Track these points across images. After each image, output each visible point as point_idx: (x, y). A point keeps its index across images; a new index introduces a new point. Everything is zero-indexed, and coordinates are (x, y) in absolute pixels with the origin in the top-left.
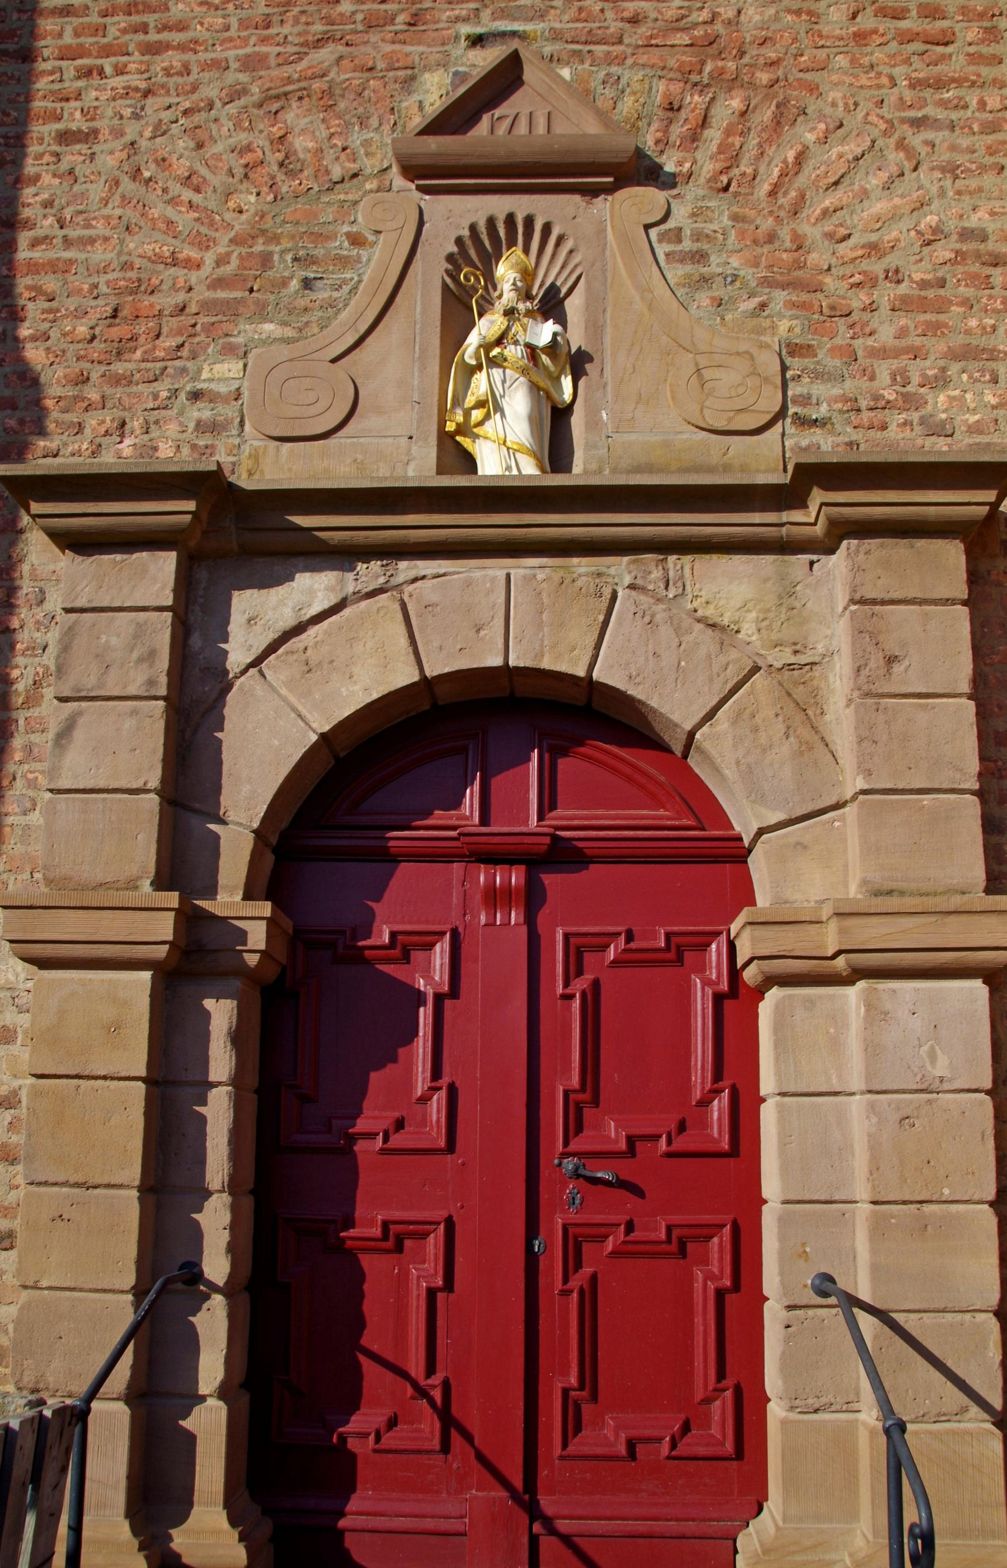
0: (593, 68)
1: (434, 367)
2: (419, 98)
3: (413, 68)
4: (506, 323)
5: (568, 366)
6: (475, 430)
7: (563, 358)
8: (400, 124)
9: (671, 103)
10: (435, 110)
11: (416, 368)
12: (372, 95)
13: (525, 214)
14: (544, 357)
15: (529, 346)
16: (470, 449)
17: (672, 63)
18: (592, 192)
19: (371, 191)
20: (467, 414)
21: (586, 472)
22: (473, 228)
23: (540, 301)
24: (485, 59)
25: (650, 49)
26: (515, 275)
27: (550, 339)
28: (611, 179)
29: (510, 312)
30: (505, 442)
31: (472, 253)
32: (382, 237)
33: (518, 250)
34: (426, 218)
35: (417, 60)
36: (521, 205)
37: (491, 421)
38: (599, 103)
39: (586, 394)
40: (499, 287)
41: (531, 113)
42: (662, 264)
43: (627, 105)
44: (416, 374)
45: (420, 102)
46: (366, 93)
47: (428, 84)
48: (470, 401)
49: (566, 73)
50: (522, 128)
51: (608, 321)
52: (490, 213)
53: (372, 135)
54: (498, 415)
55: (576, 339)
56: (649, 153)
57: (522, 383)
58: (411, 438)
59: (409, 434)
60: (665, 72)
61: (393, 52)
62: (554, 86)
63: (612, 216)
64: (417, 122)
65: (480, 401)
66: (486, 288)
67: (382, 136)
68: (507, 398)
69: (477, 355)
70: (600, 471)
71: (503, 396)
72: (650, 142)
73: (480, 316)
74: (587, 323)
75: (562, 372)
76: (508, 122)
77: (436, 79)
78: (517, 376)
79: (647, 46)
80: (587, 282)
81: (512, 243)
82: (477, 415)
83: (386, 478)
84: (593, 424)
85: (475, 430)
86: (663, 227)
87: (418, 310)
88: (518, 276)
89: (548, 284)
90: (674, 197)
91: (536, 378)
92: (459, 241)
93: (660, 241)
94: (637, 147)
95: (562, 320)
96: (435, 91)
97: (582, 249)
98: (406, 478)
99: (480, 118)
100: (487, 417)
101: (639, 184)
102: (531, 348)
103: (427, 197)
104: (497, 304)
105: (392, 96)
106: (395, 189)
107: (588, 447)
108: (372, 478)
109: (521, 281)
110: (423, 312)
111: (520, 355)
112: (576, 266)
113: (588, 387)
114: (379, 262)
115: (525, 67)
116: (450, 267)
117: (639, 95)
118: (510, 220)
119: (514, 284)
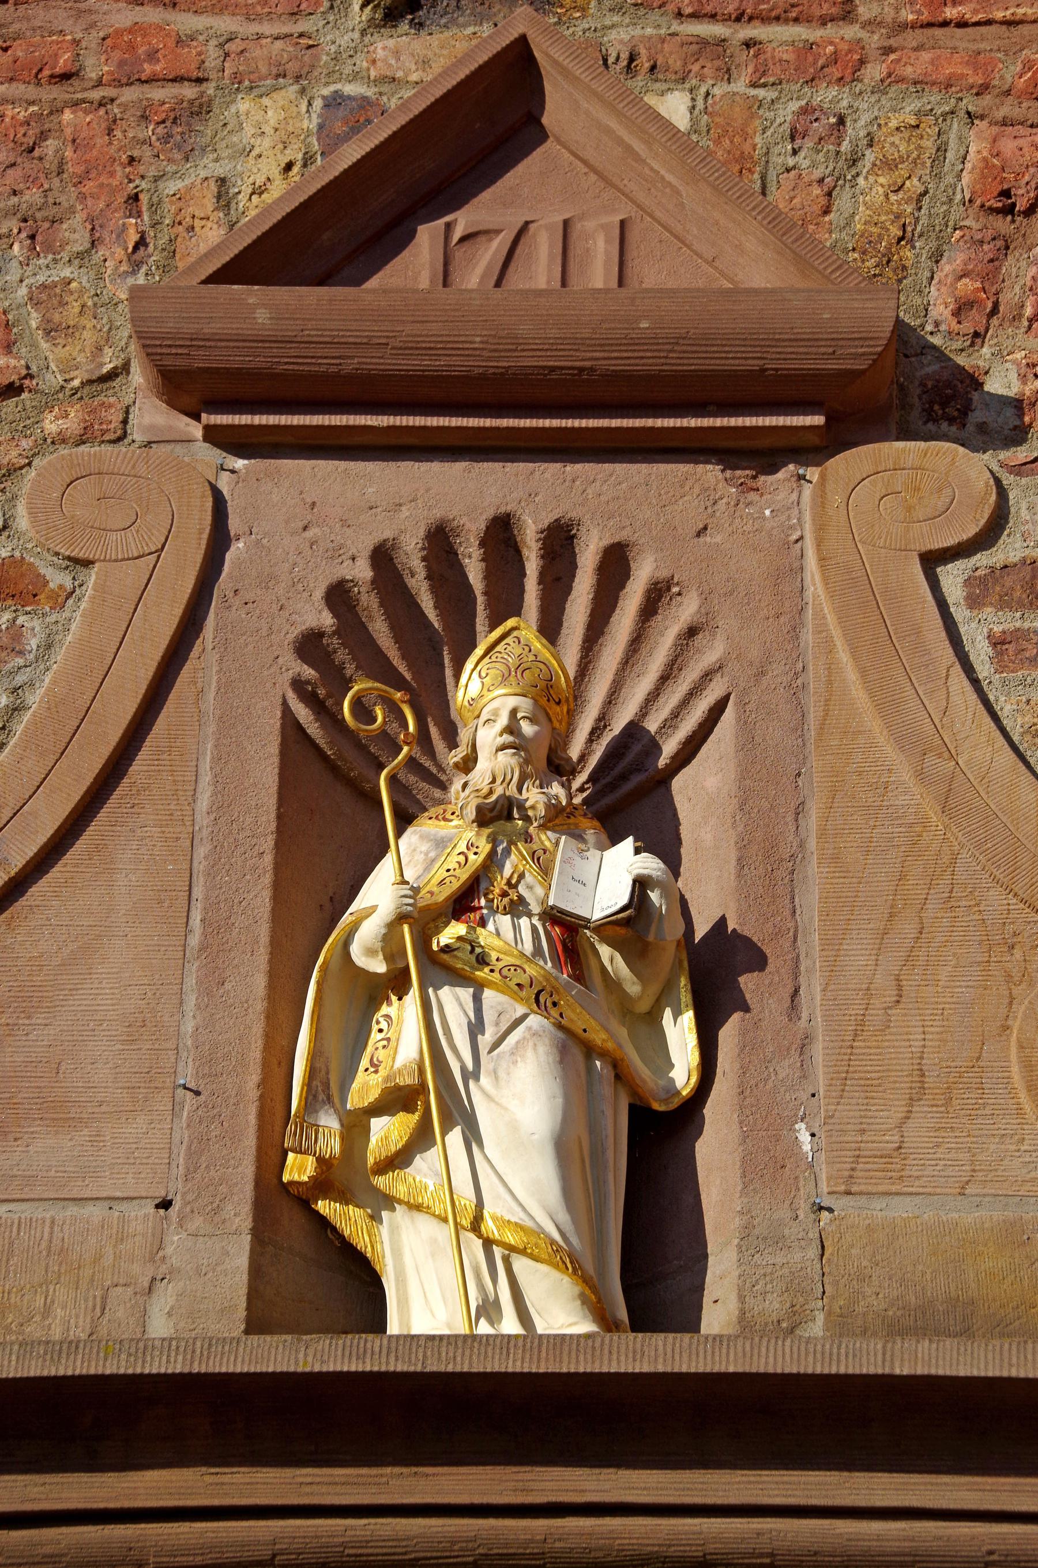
0: (761, 93)
1: (252, 979)
2: (220, 171)
3: (199, 81)
4: (485, 848)
5: (683, 981)
6: (381, 1182)
7: (669, 954)
8: (158, 242)
9: (1006, 194)
10: (268, 210)
11: (191, 981)
12: (69, 153)
14: (605, 951)
15: (554, 917)
16: (361, 1241)
17: (1010, 72)
18: (760, 456)
19: (61, 439)
20: (356, 1127)
21: (746, 1325)
22: (383, 557)
23: (593, 778)
24: (425, 63)
25: (938, 32)
26: (513, 702)
27: (624, 900)
28: (818, 420)
29: (496, 814)
30: (477, 1220)
31: (380, 630)
32: (92, 577)
33: (526, 627)
34: (234, 524)
35: (213, 54)
36: (534, 493)
37: (434, 1154)
38: (777, 196)
39: (744, 1071)
40: (464, 736)
41: (566, 223)
42: (984, 670)
43: (867, 201)
44: (191, 1001)
45: (222, 181)
46: (50, 146)
47: (249, 130)
48: (365, 1087)
49: (675, 107)
50: (539, 270)
51: (812, 844)
52: (437, 513)
53: (67, 272)
54: (455, 1137)
55: (711, 894)
56: (936, 340)
58: (165, 1204)
60: (987, 100)
61: (136, 28)
62: (638, 146)
63: (820, 529)
64: (211, 240)
65: (398, 1088)
66: (423, 738)
67: (100, 277)
68: (484, 1080)
69: (389, 943)
70: (790, 1326)
71: (472, 1075)
72: (941, 310)
73: (404, 820)
74: (743, 846)
75: (664, 997)
76: (493, 250)
77: (273, 117)
78: (520, 1010)
79: (930, 25)
80: (743, 723)
81: (505, 604)
82: (387, 1132)
83: (74, 1345)
84: (767, 1162)
85: (381, 1182)
86: (982, 560)
87: (204, 802)
88: (525, 705)
89: (618, 725)
90: (1018, 470)
91: (578, 1019)
93: (974, 602)
94: (899, 323)
95: (663, 840)
96: (268, 152)
97: (727, 622)
98: (144, 1345)
99: (412, 235)
100: (422, 1138)
101: (906, 434)
102: (567, 932)
103: (240, 463)
104: (456, 786)
105: (132, 160)
106: (137, 435)
107: (750, 1240)
108: (26, 1345)
109: (532, 720)
110: (218, 808)
111: (528, 947)
112: (707, 676)
113: (746, 1047)
114: (81, 651)
115: (548, 87)
116: (309, 673)
117: (903, 170)
118: (501, 534)
119: (512, 729)
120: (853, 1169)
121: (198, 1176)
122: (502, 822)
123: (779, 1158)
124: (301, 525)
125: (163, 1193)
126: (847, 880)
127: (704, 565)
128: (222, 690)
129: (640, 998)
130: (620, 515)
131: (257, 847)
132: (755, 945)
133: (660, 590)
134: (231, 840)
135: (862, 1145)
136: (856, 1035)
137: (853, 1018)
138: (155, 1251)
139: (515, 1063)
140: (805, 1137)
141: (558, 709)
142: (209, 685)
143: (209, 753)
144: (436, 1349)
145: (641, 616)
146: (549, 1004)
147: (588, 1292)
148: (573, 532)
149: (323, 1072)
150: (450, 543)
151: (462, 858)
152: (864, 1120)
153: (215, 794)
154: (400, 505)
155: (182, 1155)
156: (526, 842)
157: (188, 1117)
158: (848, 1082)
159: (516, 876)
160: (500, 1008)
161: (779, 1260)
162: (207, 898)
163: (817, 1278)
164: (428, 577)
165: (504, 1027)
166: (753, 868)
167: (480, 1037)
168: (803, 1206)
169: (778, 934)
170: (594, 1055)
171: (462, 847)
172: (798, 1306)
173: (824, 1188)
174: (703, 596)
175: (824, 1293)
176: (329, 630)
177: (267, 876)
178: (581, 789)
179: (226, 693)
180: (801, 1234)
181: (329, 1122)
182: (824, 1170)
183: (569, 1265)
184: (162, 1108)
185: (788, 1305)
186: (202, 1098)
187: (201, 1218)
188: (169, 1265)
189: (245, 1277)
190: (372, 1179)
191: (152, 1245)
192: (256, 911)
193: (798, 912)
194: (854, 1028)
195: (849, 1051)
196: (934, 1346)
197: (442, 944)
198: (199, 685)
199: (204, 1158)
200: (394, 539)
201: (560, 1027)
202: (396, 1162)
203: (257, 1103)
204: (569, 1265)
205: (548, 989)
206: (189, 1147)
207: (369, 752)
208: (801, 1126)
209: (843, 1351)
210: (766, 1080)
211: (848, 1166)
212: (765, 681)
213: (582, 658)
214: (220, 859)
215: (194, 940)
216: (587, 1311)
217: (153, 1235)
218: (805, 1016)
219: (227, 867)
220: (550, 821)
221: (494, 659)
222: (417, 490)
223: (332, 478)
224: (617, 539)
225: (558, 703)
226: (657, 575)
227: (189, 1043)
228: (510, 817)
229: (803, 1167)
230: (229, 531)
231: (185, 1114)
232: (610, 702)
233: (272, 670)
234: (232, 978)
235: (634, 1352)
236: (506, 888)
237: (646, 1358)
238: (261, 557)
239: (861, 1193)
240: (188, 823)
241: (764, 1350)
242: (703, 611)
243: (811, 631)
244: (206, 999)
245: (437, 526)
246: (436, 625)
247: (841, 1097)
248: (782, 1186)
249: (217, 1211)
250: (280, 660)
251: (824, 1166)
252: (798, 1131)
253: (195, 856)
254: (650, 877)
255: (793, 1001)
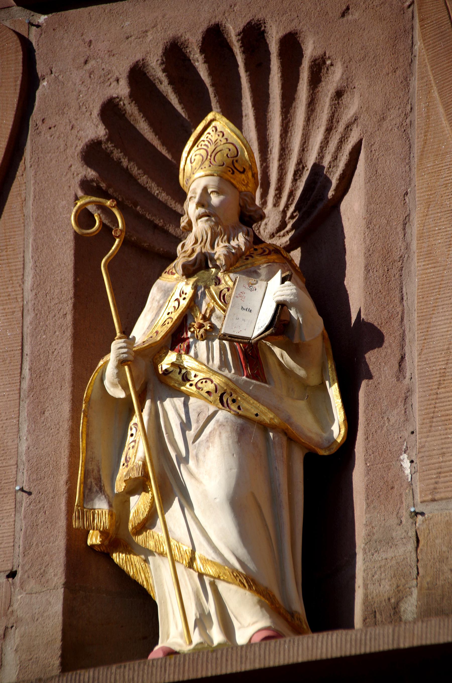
4: (189, 291)
6: (140, 539)
11: (24, 414)
13: (242, 24)
30: (192, 559)
34: (41, 68)
44: (25, 428)
51: (414, 246)
52: (171, 33)
57: (221, 425)
58: (12, 575)
59: (8, 567)
68: (192, 463)
78: (212, 409)
81: (200, 110)
82: (139, 505)
92: (110, 111)
97: (361, 83)
103: (42, 19)
109: (218, 192)
110: (38, 285)
112: (348, 128)
116: (91, 174)
120: (436, 483)
121: (32, 551)
122: (202, 271)
123: (390, 482)
124: (82, 60)
125: (10, 568)
126: (436, 269)
127: (346, 39)
128: (37, 197)
129: (308, 378)
130: (290, 10)
131: (62, 310)
132: (376, 328)
133: (319, 64)
134: (46, 308)
135: (443, 464)
136: (440, 384)
137: (438, 372)
138: (7, 608)
139: (208, 448)
140: (406, 464)
141: (243, 176)
142: (29, 195)
143: (30, 246)
144: (122, 674)
145: (310, 85)
146: (230, 402)
147: (263, 599)
148: (263, 28)
149: (96, 471)
150: (183, 53)
151: (176, 304)
152: (444, 446)
153: (35, 276)
154: (146, 31)
155: (21, 539)
156: (216, 284)
157: (25, 511)
158: (434, 420)
159: (208, 311)
160: (199, 410)
161: (390, 554)
162: (32, 353)
163: (414, 564)
164: (170, 83)
165: (201, 423)
166: (375, 270)
167: (187, 432)
168: (404, 513)
169: (391, 317)
170: (269, 430)
171: (177, 296)
172: (401, 586)
173: (418, 499)
174: (345, 65)
175: (418, 573)
176: (104, 139)
177: (69, 331)
178: (292, 217)
179: (40, 199)
180: (404, 534)
181: (101, 506)
182: (418, 486)
183: (246, 585)
184: (8, 507)
185: (395, 586)
186: (33, 496)
187: (34, 581)
188: (15, 617)
189: (60, 618)
190: (134, 538)
191: (5, 604)
192: (63, 357)
193: (405, 298)
194: (438, 379)
195: (435, 396)
196: (425, 625)
197: (164, 369)
198: (23, 196)
199: (34, 538)
200: (143, 60)
201: (238, 415)
202: (147, 525)
203: (66, 495)
204: (246, 585)
205: (228, 391)
206: (26, 532)
207: (146, 219)
208: (404, 457)
209: (368, 637)
210: (382, 427)
211: (433, 481)
212: (385, 124)
213: (283, 120)
214: (39, 323)
215: (25, 385)
216: (265, 612)
217: (6, 597)
218: (408, 375)
219: (44, 328)
220: (231, 266)
221: (200, 147)
222: (157, 17)
223: (102, 18)
224: (288, 30)
225: (243, 172)
226: (315, 54)
227: (24, 458)
228: (207, 268)
229: (405, 486)
230: (37, 74)
231: (23, 509)
232: (303, 150)
233: (68, 176)
234: (49, 408)
235: (241, 657)
236: (201, 322)
237: (248, 661)
238: (58, 91)
239: (442, 499)
240: (19, 300)
241: (320, 644)
242: (345, 77)
243: (417, 78)
244: (33, 426)
245: (171, 44)
246: (183, 115)
247: (430, 431)
248: (391, 502)
249: (43, 575)
250: (73, 167)
251: (418, 484)
252: (402, 461)
253: (25, 323)
254: (285, 301)
255: (400, 366)
